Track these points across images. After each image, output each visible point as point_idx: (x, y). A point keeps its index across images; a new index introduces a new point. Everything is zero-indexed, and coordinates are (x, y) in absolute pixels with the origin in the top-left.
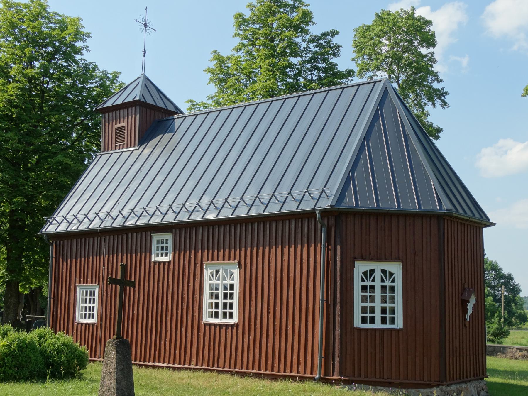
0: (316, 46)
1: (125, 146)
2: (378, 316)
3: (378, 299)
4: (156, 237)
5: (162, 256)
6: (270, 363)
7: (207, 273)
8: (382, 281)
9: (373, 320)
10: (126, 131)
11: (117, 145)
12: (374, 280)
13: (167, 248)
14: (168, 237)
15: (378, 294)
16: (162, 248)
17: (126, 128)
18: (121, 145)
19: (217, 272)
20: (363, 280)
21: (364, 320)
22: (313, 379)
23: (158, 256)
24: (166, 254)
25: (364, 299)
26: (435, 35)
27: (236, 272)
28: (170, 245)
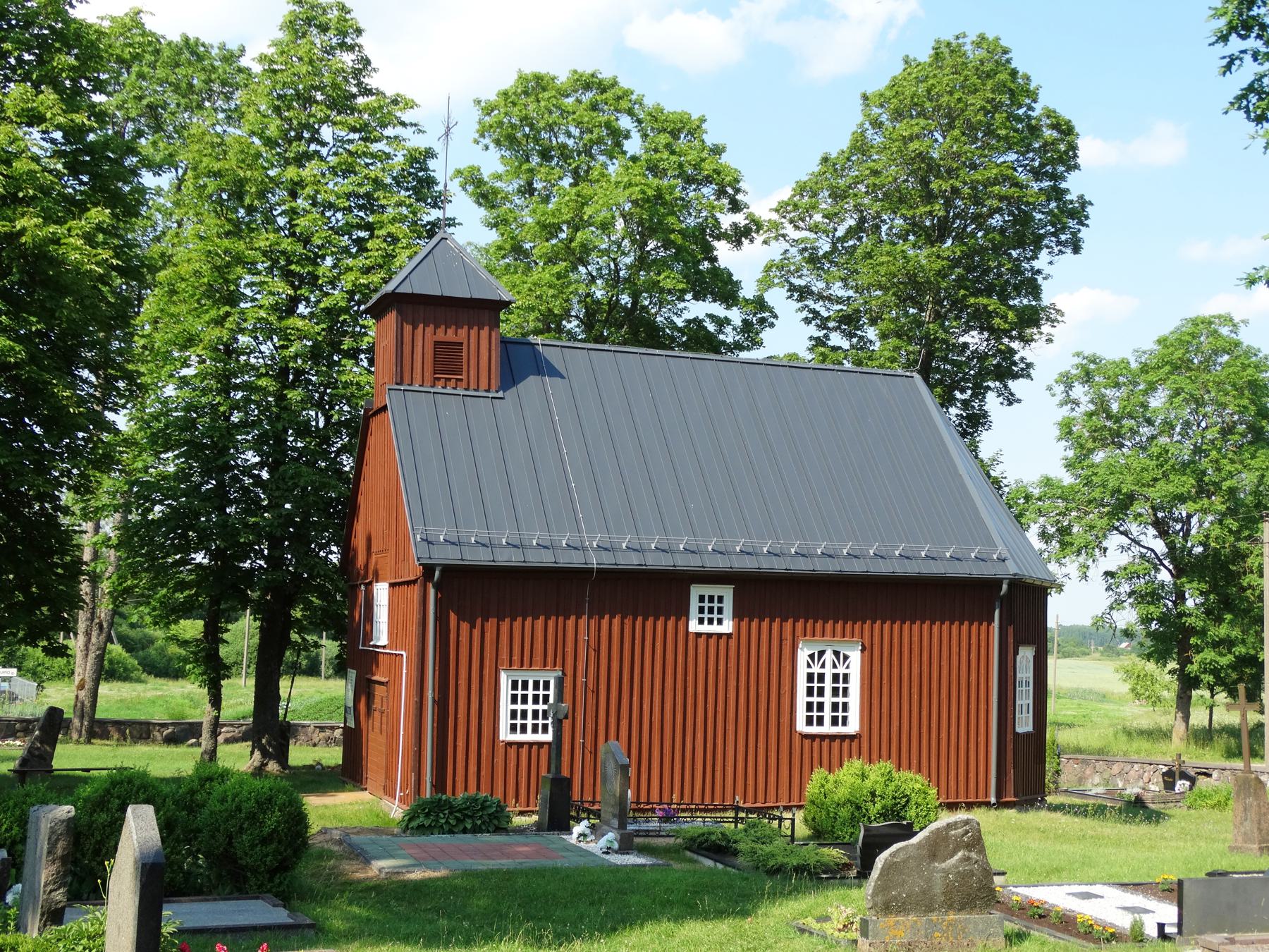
0: (966, 345)
1: (464, 384)
2: (827, 714)
3: (828, 692)
4: (696, 591)
5: (711, 621)
6: (982, 785)
7: (803, 655)
8: (835, 666)
9: (820, 721)
10: (465, 354)
11: (439, 379)
12: (823, 666)
13: (720, 611)
14: (727, 592)
15: (828, 685)
16: (711, 610)
17: (465, 347)
18: (450, 379)
19: (821, 653)
20: (809, 666)
21: (809, 721)
22: (988, 804)
23: (701, 621)
24: (720, 622)
25: (810, 692)
26: (735, 278)
27: (855, 656)
28: (728, 605)
